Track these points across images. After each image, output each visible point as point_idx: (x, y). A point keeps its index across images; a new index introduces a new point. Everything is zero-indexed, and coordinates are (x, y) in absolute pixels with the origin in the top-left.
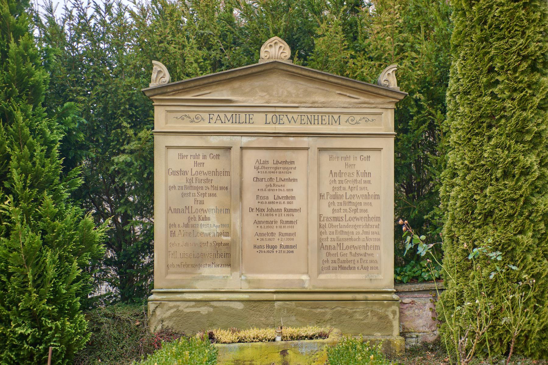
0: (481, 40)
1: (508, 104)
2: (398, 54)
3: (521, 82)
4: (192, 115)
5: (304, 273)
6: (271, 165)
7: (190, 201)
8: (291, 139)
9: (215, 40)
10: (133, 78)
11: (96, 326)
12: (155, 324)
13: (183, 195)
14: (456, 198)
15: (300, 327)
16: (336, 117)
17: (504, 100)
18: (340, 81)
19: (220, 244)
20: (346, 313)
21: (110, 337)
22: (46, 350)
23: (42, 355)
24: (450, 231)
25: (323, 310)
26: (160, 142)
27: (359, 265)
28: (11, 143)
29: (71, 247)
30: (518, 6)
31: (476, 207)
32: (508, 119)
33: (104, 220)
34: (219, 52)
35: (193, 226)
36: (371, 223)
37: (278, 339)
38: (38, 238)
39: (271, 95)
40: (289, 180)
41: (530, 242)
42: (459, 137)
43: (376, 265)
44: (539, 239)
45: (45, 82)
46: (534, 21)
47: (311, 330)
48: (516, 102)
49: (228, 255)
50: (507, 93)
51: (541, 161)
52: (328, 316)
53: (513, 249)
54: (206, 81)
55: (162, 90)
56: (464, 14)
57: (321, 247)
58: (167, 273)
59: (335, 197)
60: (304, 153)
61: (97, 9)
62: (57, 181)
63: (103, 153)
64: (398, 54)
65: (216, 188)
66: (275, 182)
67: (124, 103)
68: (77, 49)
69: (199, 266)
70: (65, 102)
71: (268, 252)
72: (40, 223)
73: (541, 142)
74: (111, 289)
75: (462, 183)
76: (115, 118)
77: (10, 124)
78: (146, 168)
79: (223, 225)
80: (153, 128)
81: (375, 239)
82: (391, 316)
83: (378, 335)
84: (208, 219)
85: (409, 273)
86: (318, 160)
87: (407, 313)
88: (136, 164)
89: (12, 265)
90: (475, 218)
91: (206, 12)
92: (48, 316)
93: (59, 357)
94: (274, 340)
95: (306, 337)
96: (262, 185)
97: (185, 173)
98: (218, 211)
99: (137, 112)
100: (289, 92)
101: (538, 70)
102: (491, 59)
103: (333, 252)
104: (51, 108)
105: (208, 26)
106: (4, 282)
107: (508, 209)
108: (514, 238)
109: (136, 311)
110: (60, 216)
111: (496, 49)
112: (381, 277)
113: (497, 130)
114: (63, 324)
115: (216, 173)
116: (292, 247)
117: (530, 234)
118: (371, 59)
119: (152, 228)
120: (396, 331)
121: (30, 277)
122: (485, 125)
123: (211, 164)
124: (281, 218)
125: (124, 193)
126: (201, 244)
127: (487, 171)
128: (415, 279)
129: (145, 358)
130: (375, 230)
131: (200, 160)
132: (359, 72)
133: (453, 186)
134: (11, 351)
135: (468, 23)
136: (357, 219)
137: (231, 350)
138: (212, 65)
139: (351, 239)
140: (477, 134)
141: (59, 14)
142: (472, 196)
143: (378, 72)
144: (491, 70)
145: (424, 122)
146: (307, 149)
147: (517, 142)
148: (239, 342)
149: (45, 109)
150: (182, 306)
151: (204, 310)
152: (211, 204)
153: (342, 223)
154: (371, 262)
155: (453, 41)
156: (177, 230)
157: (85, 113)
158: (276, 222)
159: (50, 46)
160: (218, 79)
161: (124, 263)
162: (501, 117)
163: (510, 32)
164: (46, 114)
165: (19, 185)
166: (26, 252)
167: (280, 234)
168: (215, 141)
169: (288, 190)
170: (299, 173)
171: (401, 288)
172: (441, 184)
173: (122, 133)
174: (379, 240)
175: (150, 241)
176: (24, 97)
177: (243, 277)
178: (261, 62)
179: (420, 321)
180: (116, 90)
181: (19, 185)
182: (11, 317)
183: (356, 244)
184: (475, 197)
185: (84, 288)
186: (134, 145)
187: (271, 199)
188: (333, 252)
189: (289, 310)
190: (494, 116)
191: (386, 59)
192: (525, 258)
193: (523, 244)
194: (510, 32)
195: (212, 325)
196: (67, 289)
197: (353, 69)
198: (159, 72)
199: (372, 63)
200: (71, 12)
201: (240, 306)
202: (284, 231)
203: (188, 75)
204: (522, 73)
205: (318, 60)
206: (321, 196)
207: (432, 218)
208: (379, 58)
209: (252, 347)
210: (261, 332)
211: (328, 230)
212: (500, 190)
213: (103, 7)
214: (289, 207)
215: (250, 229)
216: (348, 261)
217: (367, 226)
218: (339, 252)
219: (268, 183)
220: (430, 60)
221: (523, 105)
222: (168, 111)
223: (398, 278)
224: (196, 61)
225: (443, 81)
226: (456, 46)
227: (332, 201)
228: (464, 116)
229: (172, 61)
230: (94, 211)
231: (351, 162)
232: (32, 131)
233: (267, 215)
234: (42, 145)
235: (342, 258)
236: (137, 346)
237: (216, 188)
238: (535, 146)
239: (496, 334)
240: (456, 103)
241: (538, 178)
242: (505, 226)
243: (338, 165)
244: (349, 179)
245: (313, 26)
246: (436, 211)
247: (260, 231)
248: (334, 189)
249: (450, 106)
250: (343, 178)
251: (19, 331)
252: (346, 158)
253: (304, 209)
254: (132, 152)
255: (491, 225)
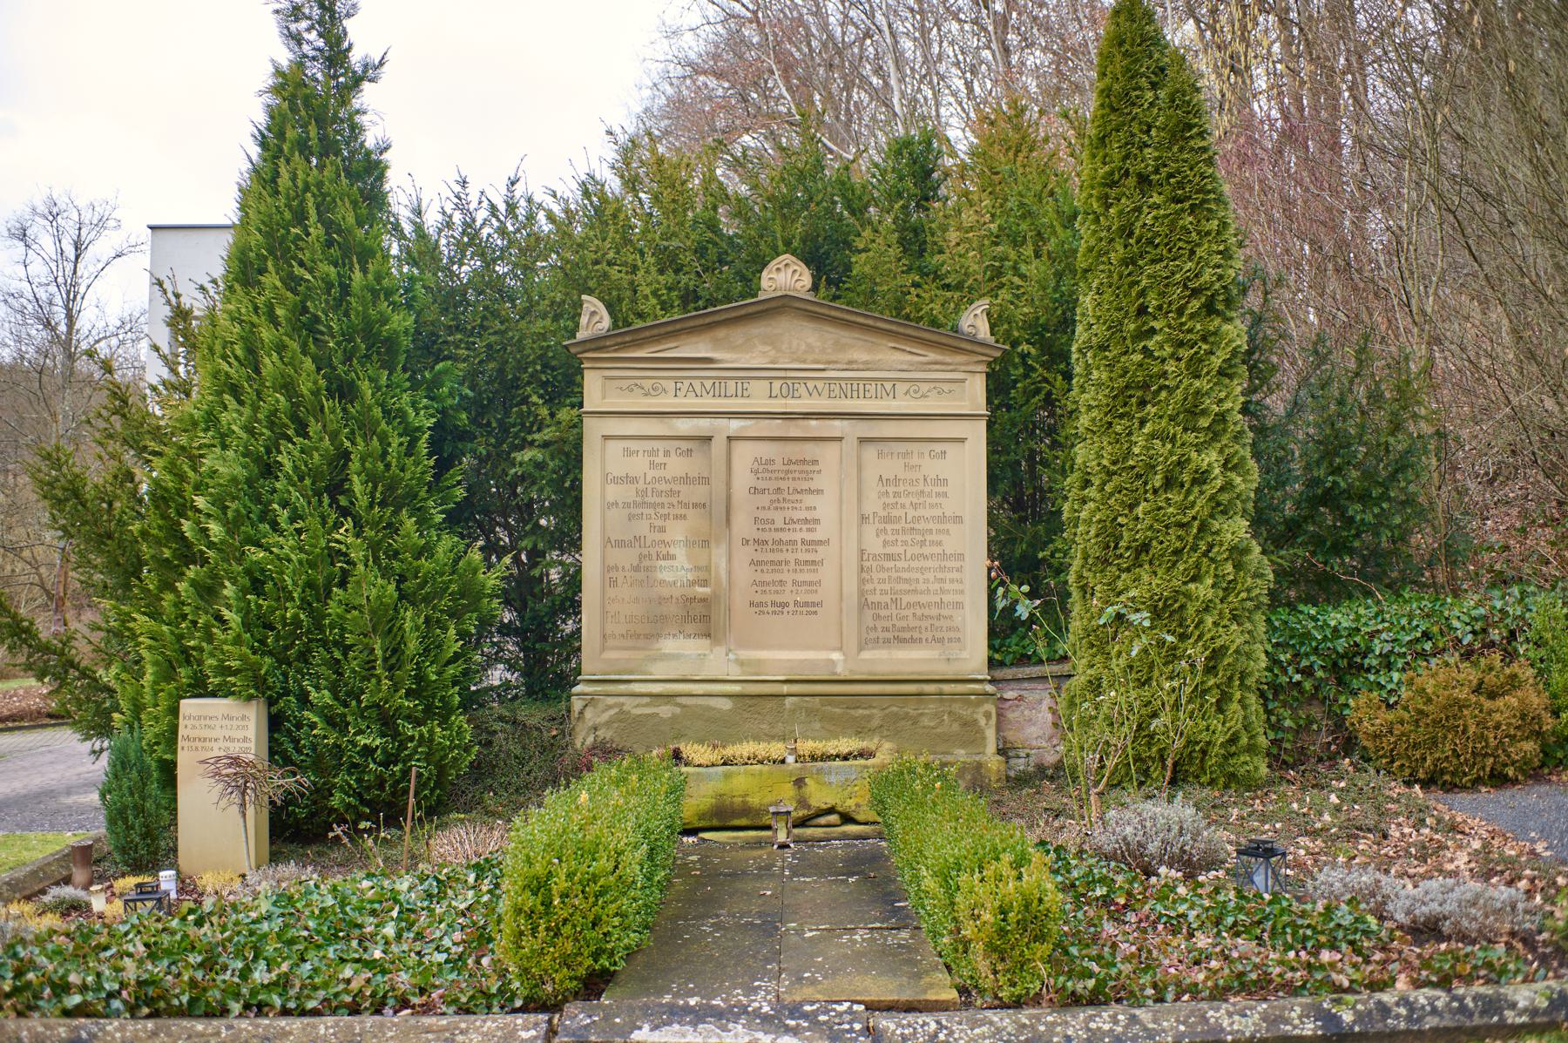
0: (1125, 262)
1: (1171, 367)
2: (991, 279)
3: (1190, 331)
4: (647, 384)
5: (834, 649)
6: (778, 466)
7: (642, 528)
8: (813, 423)
9: (686, 258)
10: (548, 322)
11: (484, 736)
12: (583, 734)
13: (631, 517)
14: (1089, 522)
15: (827, 739)
16: (888, 386)
17: (1163, 361)
18: (894, 328)
19: (692, 600)
20: (906, 717)
21: (509, 755)
22: (406, 773)
23: (398, 782)
24: (1081, 577)
25: (867, 712)
26: (593, 430)
27: (929, 635)
28: (353, 432)
29: (445, 603)
30: (1183, 210)
31: (1121, 537)
32: (1171, 391)
33: (499, 559)
34: (693, 276)
35: (647, 569)
36: (949, 564)
37: (790, 759)
38: (392, 588)
39: (779, 351)
40: (810, 491)
41: (1210, 596)
42: (1093, 420)
43: (957, 635)
44: (1225, 590)
45: (406, 332)
46: (1208, 233)
47: (845, 745)
48: (1183, 364)
49: (706, 618)
50: (1168, 349)
51: (1227, 461)
52: (875, 723)
53: (1182, 607)
54: (669, 329)
55: (597, 343)
56: (1097, 220)
57: (863, 604)
58: (603, 649)
59: (888, 519)
60: (835, 445)
61: (493, 209)
62: (423, 494)
63: (500, 443)
64: (991, 279)
65: (686, 506)
66: (786, 495)
67: (534, 363)
68: (458, 276)
69: (657, 636)
70: (437, 361)
71: (774, 613)
72: (395, 564)
73: (1225, 430)
74: (508, 676)
75: (1098, 496)
76: (518, 387)
77: (352, 402)
78: (568, 472)
79: (697, 568)
80: (581, 405)
81: (956, 592)
82: (983, 722)
83: (961, 755)
84: (673, 557)
85: (1014, 648)
86: (859, 458)
87: (1011, 715)
88: (551, 464)
89: (351, 632)
90: (1121, 556)
91: (674, 211)
92: (408, 718)
93: (425, 785)
94: (783, 761)
95: (837, 756)
96: (765, 500)
97: (634, 480)
98: (689, 544)
99: (554, 377)
100: (809, 345)
101: (1218, 313)
102: (1142, 294)
103: (883, 613)
104: (414, 373)
105: (674, 234)
106: (338, 661)
107: (1172, 539)
108: (1183, 588)
109: (551, 711)
110: (426, 551)
111: (1149, 277)
112: (965, 655)
113: (1154, 410)
114: (431, 732)
115: (686, 480)
116: (814, 604)
117: (1209, 581)
118: (947, 287)
119: (579, 571)
120: (991, 748)
121: (379, 652)
122: (1134, 400)
123: (677, 466)
124: (795, 556)
125: (531, 514)
126: (661, 600)
127: (1139, 476)
128: (1024, 659)
129: (567, 786)
130: (955, 575)
131: (660, 459)
132: (926, 309)
133: (1084, 501)
134: (350, 774)
135: (1103, 234)
136: (926, 557)
137: (709, 777)
138: (681, 297)
139: (915, 591)
140: (1121, 416)
141: (432, 220)
142: (1115, 519)
143: (957, 310)
144: (1142, 310)
145: (1037, 391)
146: (840, 439)
147: (1185, 430)
148: (725, 764)
149: (407, 375)
150: (629, 704)
151: (665, 711)
152: (677, 532)
153: (899, 564)
154: (950, 629)
155: (1081, 263)
156: (620, 575)
157: (471, 378)
158: (787, 563)
159: (416, 271)
160: (691, 323)
161: (532, 631)
162: (1161, 388)
163: (1170, 251)
164: (408, 384)
165: (363, 501)
166: (373, 612)
167: (794, 583)
168: (684, 426)
169: (808, 509)
170: (826, 480)
171: (1000, 673)
172: (1066, 498)
173: (529, 413)
174: (962, 592)
175: (575, 594)
176: (375, 358)
177: (731, 656)
178: (762, 296)
179: (1033, 729)
180: (520, 341)
181: (363, 501)
182: (349, 718)
183: (924, 599)
184: (1120, 520)
185: (466, 673)
186: (547, 434)
187: (779, 524)
188: (883, 613)
189: (810, 712)
190: (1149, 387)
191: (971, 288)
192: (1201, 622)
193: (1197, 598)
194: (1170, 251)
195: (680, 736)
196: (439, 674)
197: (916, 304)
198: (593, 313)
199: (949, 294)
200: (450, 217)
201: (726, 705)
202: (801, 577)
203: (641, 316)
204: (1192, 316)
205: (859, 289)
206: (863, 519)
207: (1052, 556)
208: (959, 286)
209: (746, 772)
210: (761, 749)
211: (875, 576)
212: (1160, 508)
213: (502, 207)
214: (809, 536)
215: (744, 574)
216: (909, 629)
217: (942, 569)
218: (895, 612)
219: (774, 497)
220: (1044, 289)
221: (1195, 368)
222: (606, 378)
223: (997, 656)
224: (655, 293)
225: (1067, 324)
226: (1086, 271)
227: (882, 526)
228: (1100, 385)
229: (615, 293)
230: (481, 543)
231: (915, 460)
232: (386, 412)
233: (772, 551)
234: (400, 435)
235: (900, 624)
236: (552, 770)
237: (686, 506)
238: (1216, 437)
239: (1154, 749)
240: (1088, 365)
241: (1222, 489)
242: (1168, 569)
243: (891, 467)
244: (911, 489)
245: (849, 233)
246: (1059, 544)
247: (760, 577)
248: (885, 506)
249: (1078, 370)
250: (901, 488)
251: (363, 740)
252: (906, 454)
253: (834, 542)
254: (546, 445)
255: (1147, 566)
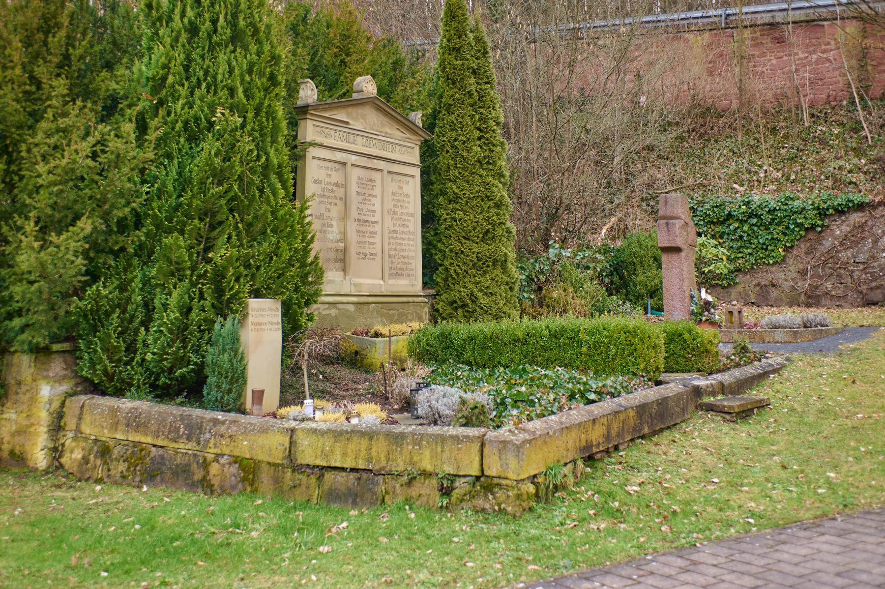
4: (326, 131)
151: (333, 312)
222: (314, 125)
248: (395, 206)
252: (399, 181)
